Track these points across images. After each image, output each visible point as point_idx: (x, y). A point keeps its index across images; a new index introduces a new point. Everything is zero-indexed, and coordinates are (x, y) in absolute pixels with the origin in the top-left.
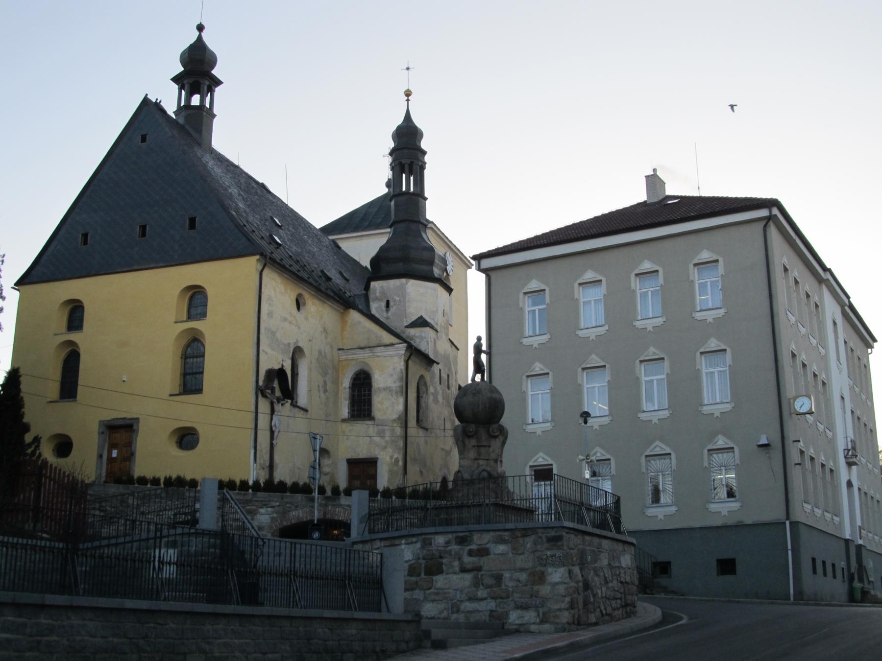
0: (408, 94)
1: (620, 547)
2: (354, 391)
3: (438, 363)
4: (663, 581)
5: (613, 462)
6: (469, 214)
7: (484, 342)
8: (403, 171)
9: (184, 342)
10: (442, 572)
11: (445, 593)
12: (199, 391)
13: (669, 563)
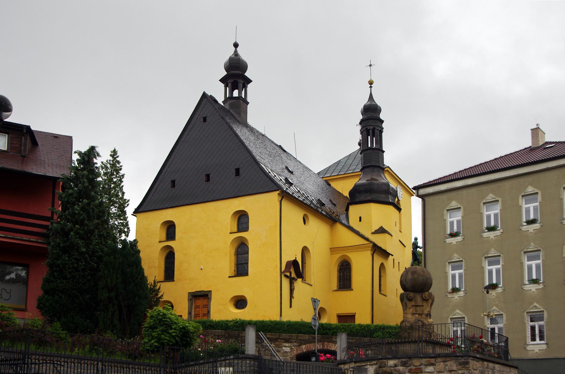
0: (371, 83)
2: (340, 273)
5: (504, 316)
7: (420, 244)
8: (368, 135)
9: (236, 245)
12: (246, 274)
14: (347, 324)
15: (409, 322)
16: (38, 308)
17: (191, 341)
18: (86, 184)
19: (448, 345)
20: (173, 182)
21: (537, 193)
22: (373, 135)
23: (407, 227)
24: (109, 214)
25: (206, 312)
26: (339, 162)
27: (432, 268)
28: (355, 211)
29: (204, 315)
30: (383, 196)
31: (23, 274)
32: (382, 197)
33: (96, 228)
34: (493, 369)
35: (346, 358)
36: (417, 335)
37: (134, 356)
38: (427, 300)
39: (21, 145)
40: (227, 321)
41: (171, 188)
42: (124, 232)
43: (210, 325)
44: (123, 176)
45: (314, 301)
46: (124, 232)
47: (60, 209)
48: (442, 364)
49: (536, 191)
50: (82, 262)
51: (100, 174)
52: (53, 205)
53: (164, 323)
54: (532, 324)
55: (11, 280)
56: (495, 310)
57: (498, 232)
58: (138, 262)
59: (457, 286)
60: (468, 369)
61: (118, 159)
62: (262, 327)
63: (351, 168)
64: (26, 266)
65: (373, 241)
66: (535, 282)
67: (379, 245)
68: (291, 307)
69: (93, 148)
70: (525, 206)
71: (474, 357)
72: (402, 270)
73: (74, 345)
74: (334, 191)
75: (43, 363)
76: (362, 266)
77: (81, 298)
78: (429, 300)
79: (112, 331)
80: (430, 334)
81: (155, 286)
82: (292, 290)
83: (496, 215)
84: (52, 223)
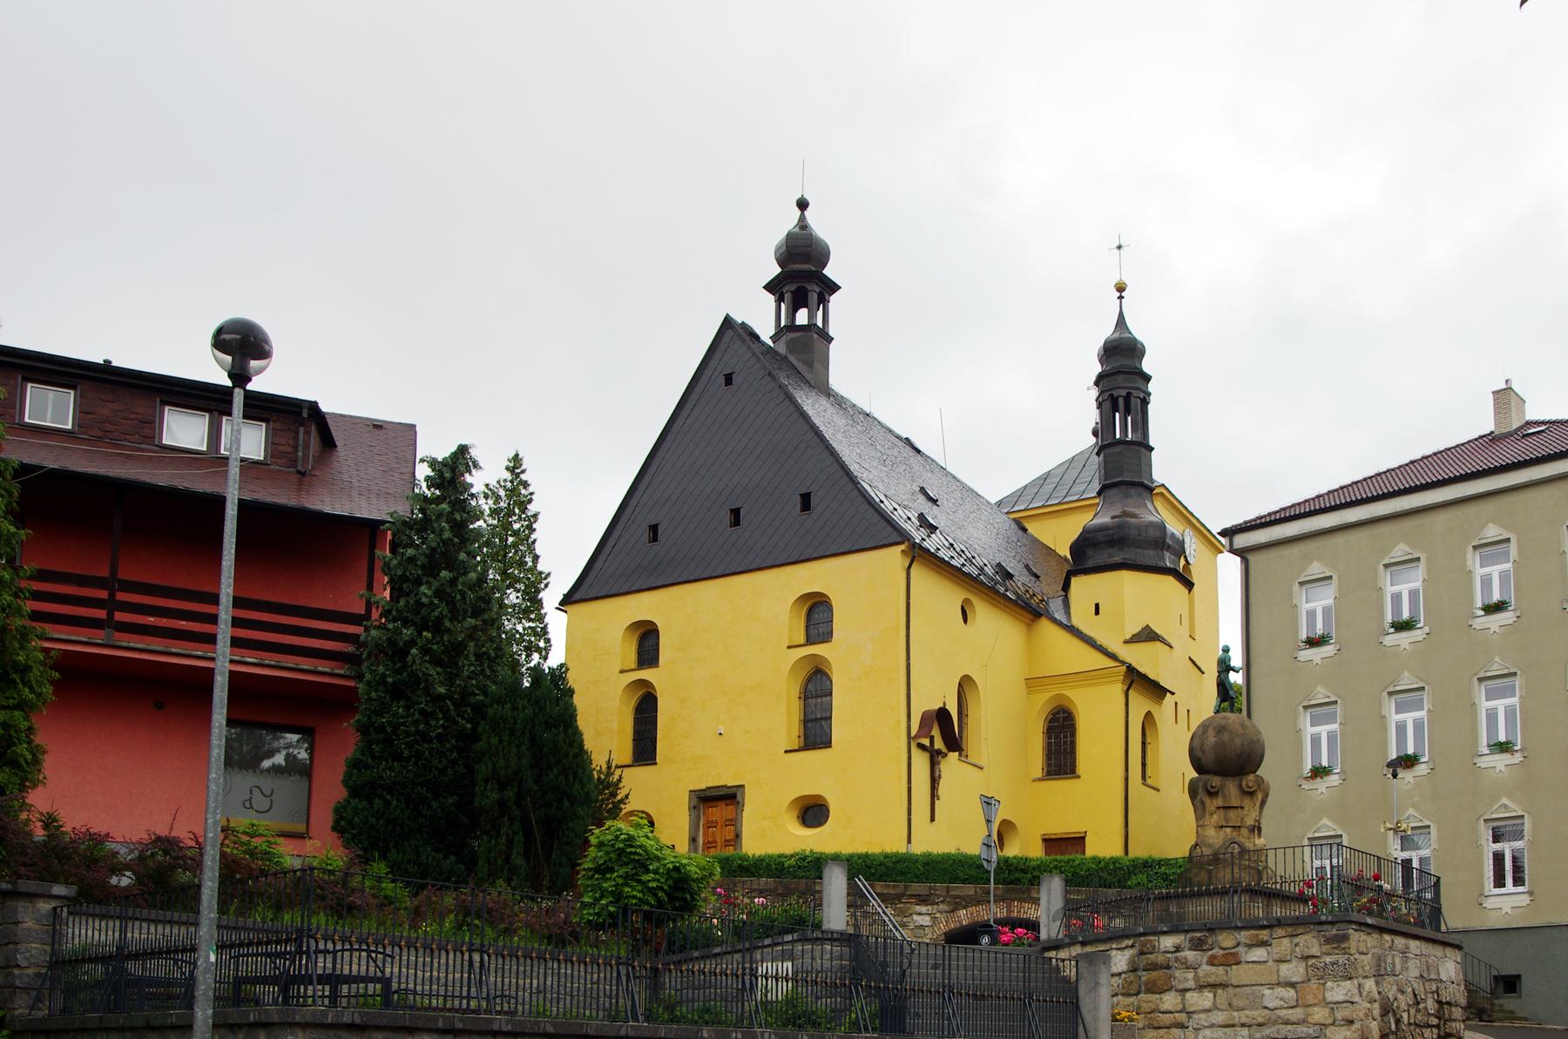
0: (1121, 288)
1: (1438, 951)
4: (1508, 1002)
5: (1433, 830)
6: (1211, 465)
7: (1237, 660)
8: (1115, 409)
9: (802, 676)
12: (827, 744)
13: (1519, 977)
14: (1066, 857)
15: (1210, 846)
16: (334, 829)
17: (694, 899)
18: (447, 535)
19: (1301, 899)
20: (654, 529)
21: (1508, 540)
22: (1127, 411)
23: (1198, 624)
24: (502, 606)
25: (732, 836)
26: (1045, 477)
27: (1266, 721)
28: (1082, 587)
29: (727, 843)
30: (1151, 553)
31: (303, 755)
32: (1149, 556)
33: (471, 637)
34: (1404, 952)
36: (1228, 877)
37: (561, 939)
38: (1251, 794)
39: (296, 448)
40: (780, 856)
41: (648, 544)
42: (538, 650)
43: (740, 866)
44: (535, 516)
45: (987, 802)
46: (538, 650)
47: (387, 594)
48: (1286, 941)
49: (1506, 536)
50: (438, 720)
51: (482, 513)
52: (370, 587)
53: (631, 858)
54: (1497, 847)
55: (276, 769)
56: (1411, 817)
57: (1418, 632)
58: (567, 719)
59: (1325, 763)
60: (1346, 952)
61: (523, 477)
62: (863, 868)
63: (1079, 488)
64: (308, 733)
65: (1128, 660)
66: (1504, 747)
67: (1142, 670)
68: (932, 820)
69: (463, 450)
70: (1479, 572)
71: (1361, 924)
72: (1194, 725)
73: (417, 915)
74: (1035, 541)
75: (343, 950)
76: (1101, 719)
77: (434, 804)
78: (1257, 793)
79: (509, 881)
80: (1260, 873)
81: (609, 774)
82: (934, 781)
83: (1413, 595)
84: (367, 629)
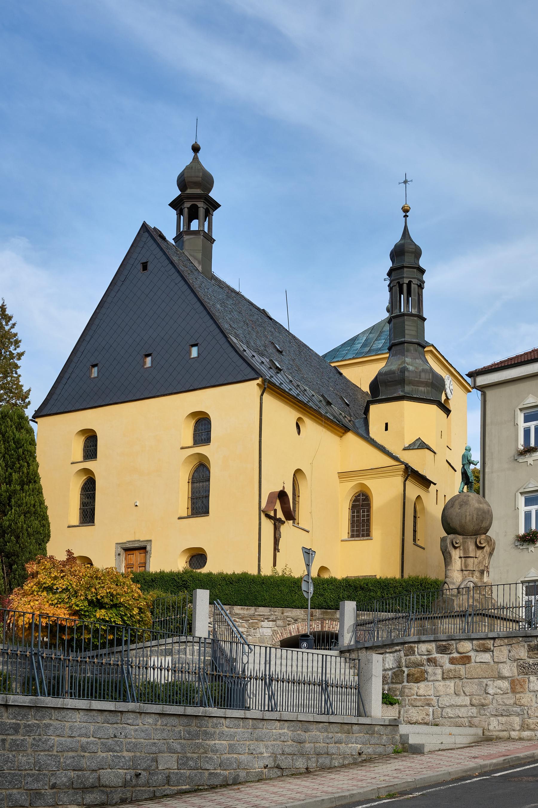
0: (406, 211)
2: (353, 512)
3: (435, 484)
6: (459, 332)
7: (476, 456)
10: (426, 679)
11: (428, 700)
28: (378, 413)
35: (352, 643)
